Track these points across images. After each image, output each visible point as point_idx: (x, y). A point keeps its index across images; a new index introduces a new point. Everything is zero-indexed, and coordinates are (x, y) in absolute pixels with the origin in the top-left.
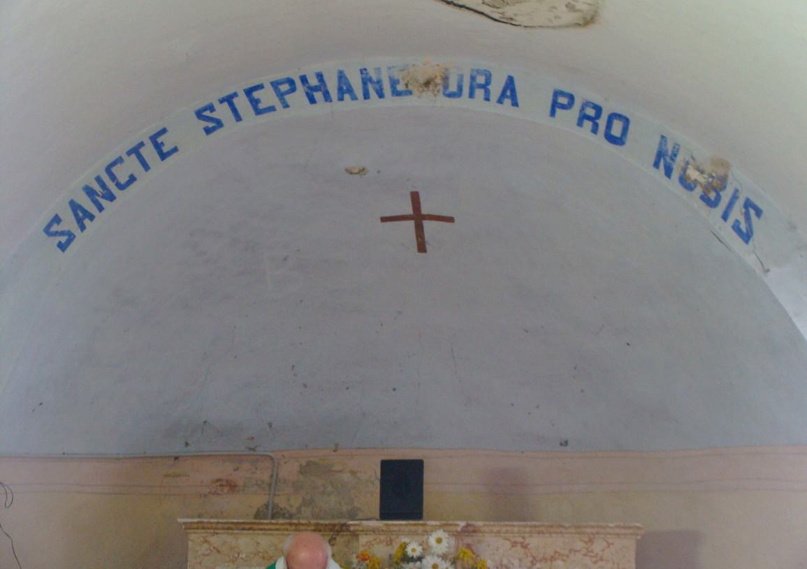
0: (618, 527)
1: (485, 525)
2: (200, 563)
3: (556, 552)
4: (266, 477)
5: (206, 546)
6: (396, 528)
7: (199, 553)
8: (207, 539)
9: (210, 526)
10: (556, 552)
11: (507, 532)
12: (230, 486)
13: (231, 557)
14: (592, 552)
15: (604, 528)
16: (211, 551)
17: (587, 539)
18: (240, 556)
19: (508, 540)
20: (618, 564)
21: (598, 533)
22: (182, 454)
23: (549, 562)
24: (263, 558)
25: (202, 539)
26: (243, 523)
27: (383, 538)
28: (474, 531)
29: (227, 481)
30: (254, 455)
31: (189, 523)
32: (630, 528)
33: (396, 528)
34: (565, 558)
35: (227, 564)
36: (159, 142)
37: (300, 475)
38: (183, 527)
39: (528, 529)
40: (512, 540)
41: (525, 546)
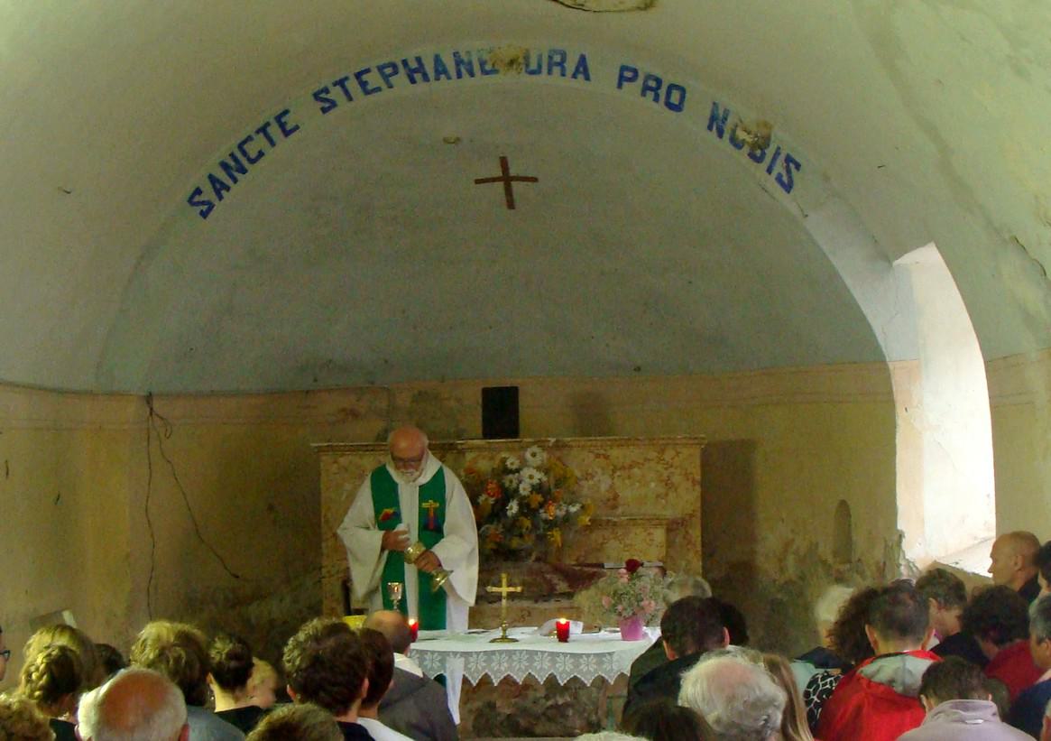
5: (335, 465)
6: (497, 446)
11: (591, 446)
21: (668, 444)
26: (367, 446)
32: (696, 438)
41: (606, 457)
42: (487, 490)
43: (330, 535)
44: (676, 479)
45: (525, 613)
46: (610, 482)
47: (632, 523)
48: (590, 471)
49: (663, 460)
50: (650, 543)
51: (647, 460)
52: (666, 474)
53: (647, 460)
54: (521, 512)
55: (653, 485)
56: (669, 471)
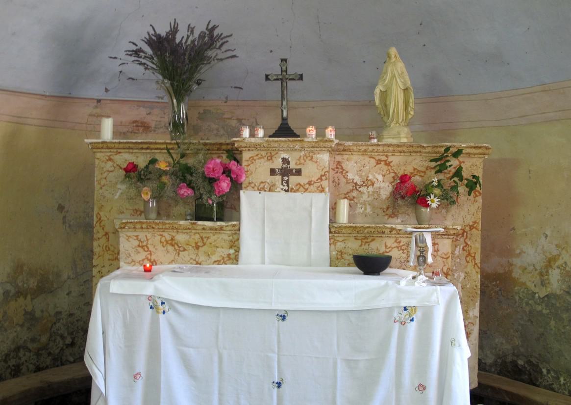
1: (353, 145)
2: (105, 178)
3: (415, 169)
5: (110, 163)
6: (276, 145)
7: (105, 169)
8: (111, 157)
9: (113, 145)
10: (415, 169)
11: (373, 151)
12: (144, 126)
16: (115, 167)
25: (107, 158)
26: (141, 143)
27: (264, 153)
28: (344, 150)
29: (142, 123)
30: (162, 102)
31: (95, 143)
32: (480, 148)
33: (276, 145)
36: (203, 112)
37: (199, 121)
38: (90, 147)
39: (391, 149)
41: (388, 164)
43: (102, 233)
48: (371, 177)
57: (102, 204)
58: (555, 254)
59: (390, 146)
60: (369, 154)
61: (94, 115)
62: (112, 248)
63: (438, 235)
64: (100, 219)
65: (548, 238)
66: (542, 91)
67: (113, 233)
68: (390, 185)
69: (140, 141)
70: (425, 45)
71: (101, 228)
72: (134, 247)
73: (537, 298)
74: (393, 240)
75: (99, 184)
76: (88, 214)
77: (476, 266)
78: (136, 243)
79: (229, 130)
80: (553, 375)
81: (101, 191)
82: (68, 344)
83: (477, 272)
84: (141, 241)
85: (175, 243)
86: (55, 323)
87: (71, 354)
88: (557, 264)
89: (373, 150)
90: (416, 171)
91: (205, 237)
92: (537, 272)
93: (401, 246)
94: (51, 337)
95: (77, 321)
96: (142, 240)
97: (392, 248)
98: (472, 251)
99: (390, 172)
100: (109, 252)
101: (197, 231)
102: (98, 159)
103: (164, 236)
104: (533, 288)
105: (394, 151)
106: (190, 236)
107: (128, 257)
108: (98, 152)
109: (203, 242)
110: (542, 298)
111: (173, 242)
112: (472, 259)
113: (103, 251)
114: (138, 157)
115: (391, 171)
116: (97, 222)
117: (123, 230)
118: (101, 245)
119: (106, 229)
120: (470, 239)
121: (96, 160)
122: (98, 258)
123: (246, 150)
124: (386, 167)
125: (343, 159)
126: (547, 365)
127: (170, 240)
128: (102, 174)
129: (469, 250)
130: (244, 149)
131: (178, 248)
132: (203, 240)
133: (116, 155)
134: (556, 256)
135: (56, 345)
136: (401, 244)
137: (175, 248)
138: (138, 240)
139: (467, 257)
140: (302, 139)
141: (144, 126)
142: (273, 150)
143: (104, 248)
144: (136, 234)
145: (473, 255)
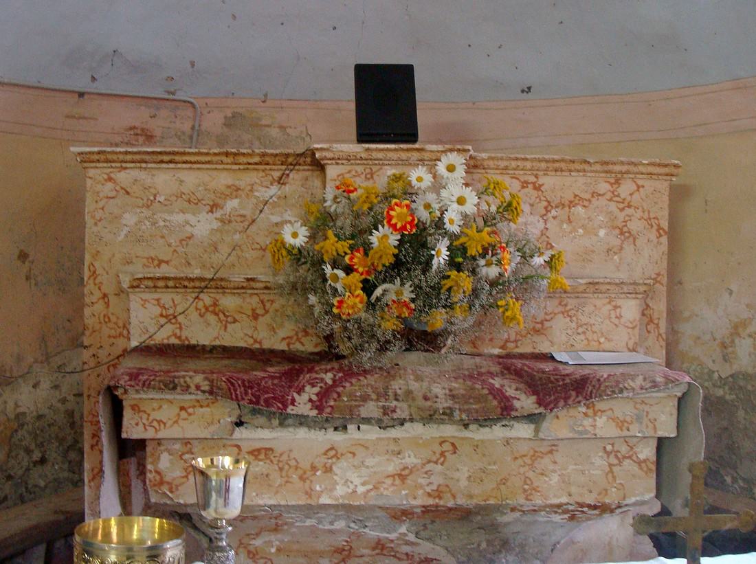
0: (653, 164)
2: (103, 209)
3: (576, 196)
4: (187, 127)
5: (110, 185)
6: (380, 155)
8: (112, 175)
12: (146, 135)
13: (145, 200)
14: (618, 196)
15: (635, 165)
17: (613, 181)
18: (158, 199)
19: (518, 179)
20: (649, 212)
21: (628, 172)
22: (89, 90)
23: (567, 209)
24: (189, 201)
25: (106, 177)
26: (160, 153)
27: (360, 169)
29: (143, 130)
31: (86, 153)
32: (666, 166)
33: (380, 155)
34: (586, 203)
35: (138, 210)
39: (543, 165)
40: (522, 180)
41: (537, 188)
42: (390, 218)
43: (98, 294)
44: (635, 226)
45: (447, 446)
46: (541, 225)
47: (592, 288)
49: (618, 196)
50: (616, 321)
51: (595, 194)
52: (621, 216)
53: (595, 194)
54: (453, 264)
55: (602, 233)
56: (624, 213)
57: (98, 249)
58: (746, 317)
59: (542, 161)
60: (510, 172)
61: (73, 117)
62: (113, 319)
63: (622, 293)
64: (94, 272)
65: (734, 295)
66: (733, 89)
67: (116, 295)
68: (541, 219)
69: (159, 150)
70: (561, 22)
71: (97, 287)
72: (153, 317)
73: (717, 378)
74: (556, 302)
75: (93, 217)
76: (63, 265)
77: (660, 337)
78: (157, 310)
79: (268, 142)
80: (742, 484)
81: (95, 229)
82: (36, 461)
83: (661, 346)
84: (165, 308)
85: (220, 311)
86: (16, 431)
87: (40, 476)
88: (748, 331)
89: (518, 166)
90: (578, 198)
91: (268, 301)
92: (717, 342)
93: (568, 311)
94: (10, 451)
95: (49, 425)
96: (166, 306)
97: (555, 314)
98: (655, 316)
99: (540, 200)
100: (109, 325)
101: (256, 291)
102: (90, 178)
103: (203, 300)
104: (710, 365)
105: (547, 169)
106: (244, 298)
107: (144, 333)
108: (92, 168)
109: (264, 309)
110: (724, 379)
111: (217, 309)
112: (654, 328)
113: (100, 323)
114: (153, 175)
115: (542, 198)
116: (89, 279)
117: (137, 290)
118: (96, 314)
119: (105, 289)
120: (652, 299)
121: (88, 180)
122: (90, 336)
123: (332, 164)
124: (536, 192)
125: (473, 180)
126: (732, 472)
127: (211, 306)
128: (96, 202)
129: (650, 315)
130: (329, 162)
131: (225, 319)
132: (264, 306)
133: (119, 172)
134: (745, 320)
135: (19, 463)
136: (568, 308)
137: (220, 319)
138: (160, 306)
139: (648, 324)
140: (422, 146)
141: (146, 135)
142: (376, 164)
143: (102, 318)
144: (156, 296)
145: (656, 322)
